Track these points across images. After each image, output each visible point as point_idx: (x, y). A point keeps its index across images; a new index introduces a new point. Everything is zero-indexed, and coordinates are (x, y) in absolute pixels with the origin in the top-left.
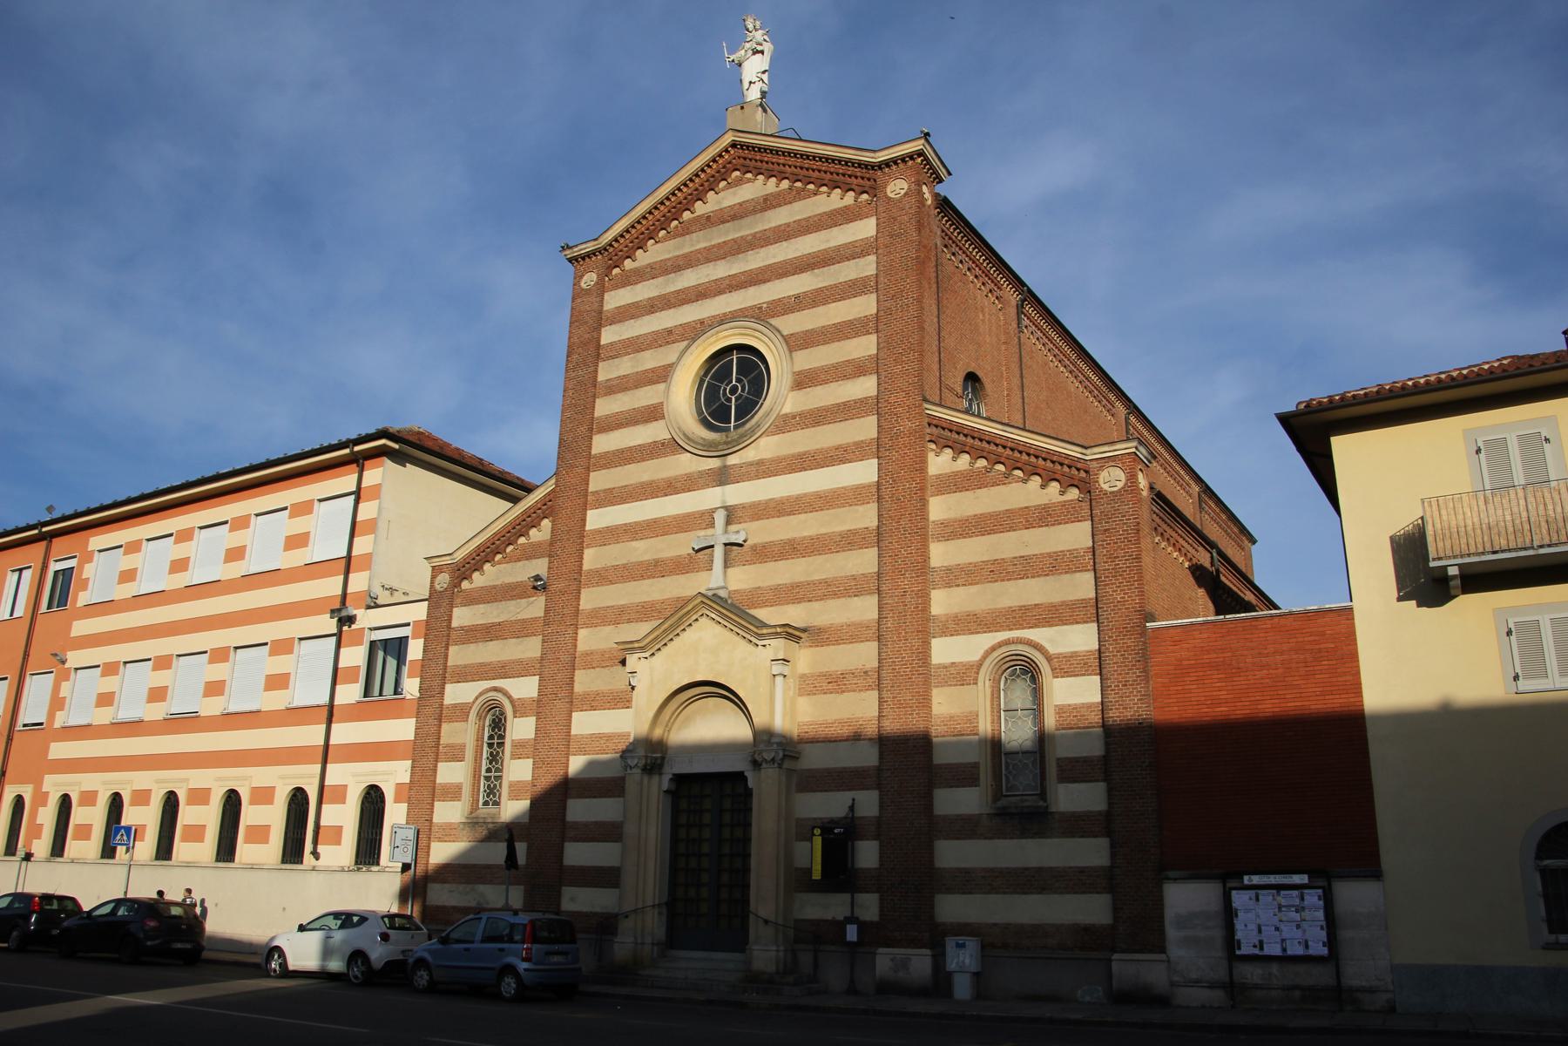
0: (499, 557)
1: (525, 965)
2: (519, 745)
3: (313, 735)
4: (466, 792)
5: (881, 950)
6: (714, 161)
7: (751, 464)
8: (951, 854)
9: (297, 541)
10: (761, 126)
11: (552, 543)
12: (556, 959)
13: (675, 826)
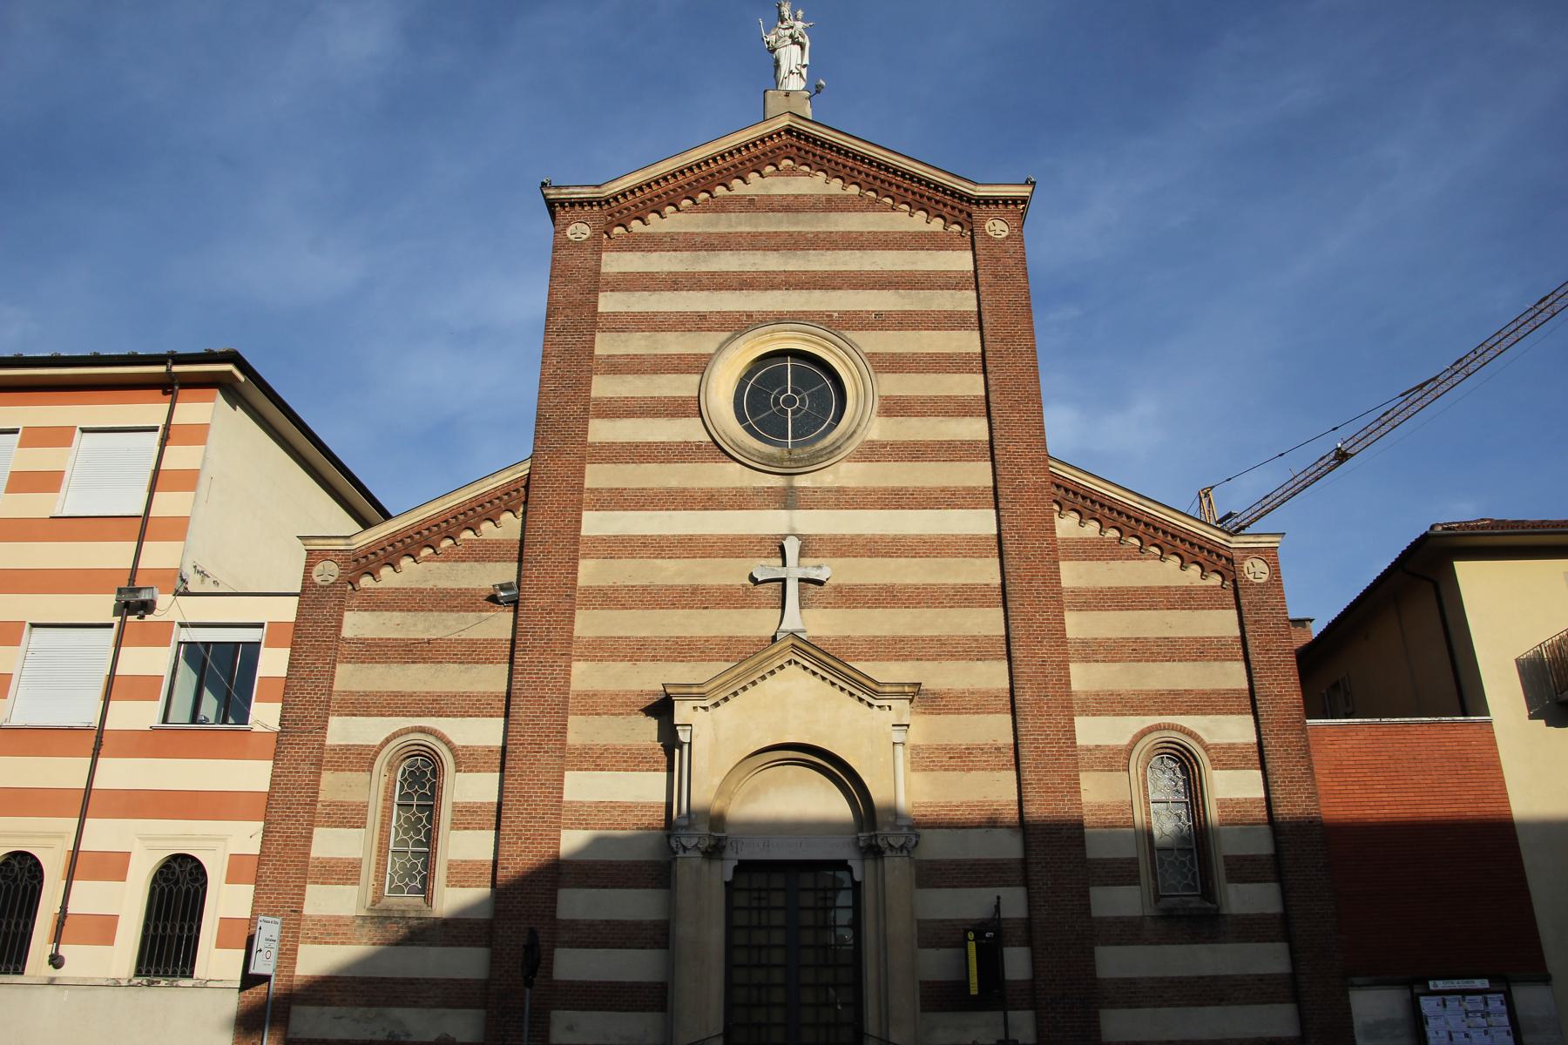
3: (68, 772)
4: (368, 873)
6: (762, 141)
7: (829, 490)
8: (1113, 962)
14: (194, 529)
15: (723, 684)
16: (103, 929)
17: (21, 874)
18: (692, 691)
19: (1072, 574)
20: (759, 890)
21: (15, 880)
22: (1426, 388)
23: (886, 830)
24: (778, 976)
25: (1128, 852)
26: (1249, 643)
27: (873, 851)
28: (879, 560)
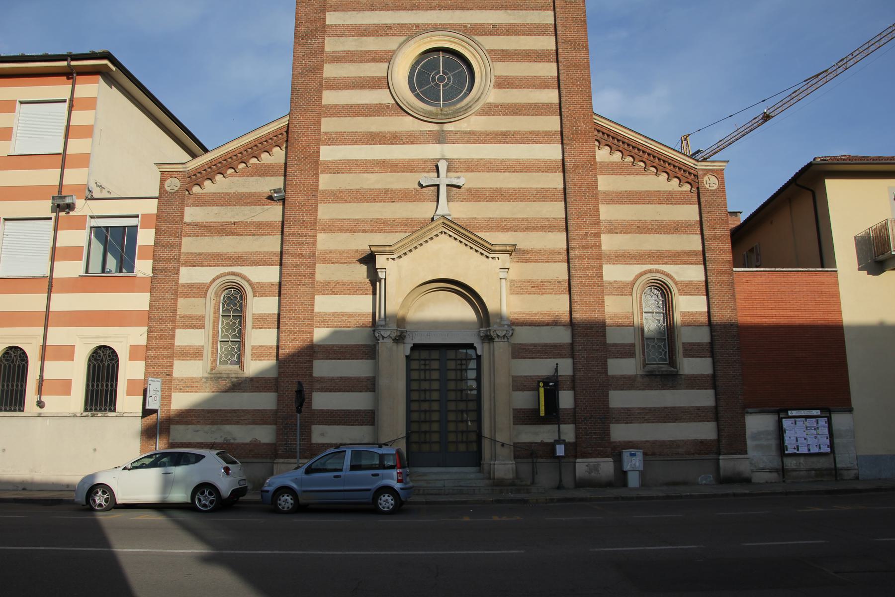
3: (35, 302)
4: (207, 353)
7: (464, 132)
8: (618, 399)
14: (93, 160)
16: (65, 387)
17: (16, 359)
18: (387, 250)
19: (605, 183)
20: (425, 360)
21: (13, 362)
22: (820, 77)
23: (496, 327)
24: (435, 427)
25: (629, 339)
26: (704, 224)
27: (488, 339)
28: (494, 173)
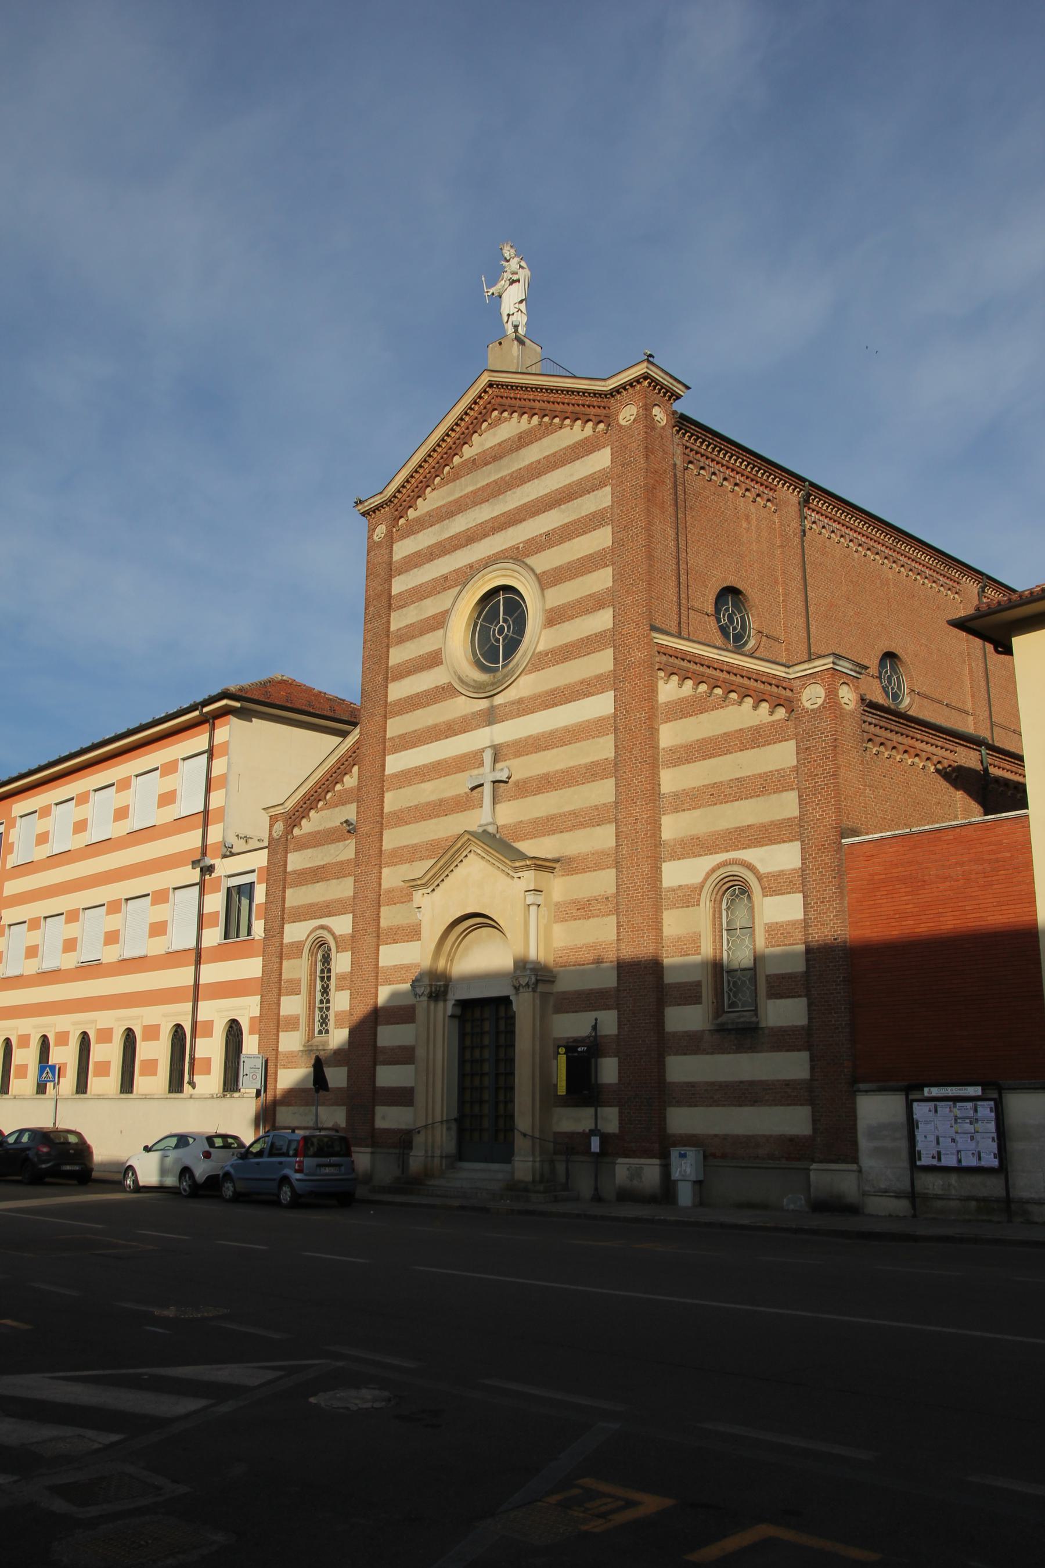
0: (321, 804)
1: (298, 1176)
2: (341, 977)
3: (183, 976)
5: (620, 1160)
6: (475, 403)
7: (513, 703)
8: (681, 1069)
9: (167, 799)
10: (508, 361)
11: (359, 788)
12: (327, 1170)
13: (462, 1048)
15: (434, 875)
